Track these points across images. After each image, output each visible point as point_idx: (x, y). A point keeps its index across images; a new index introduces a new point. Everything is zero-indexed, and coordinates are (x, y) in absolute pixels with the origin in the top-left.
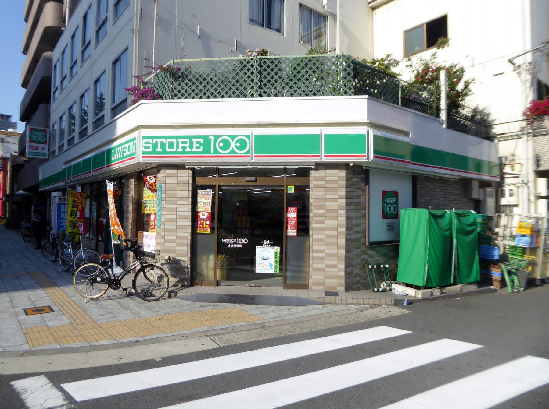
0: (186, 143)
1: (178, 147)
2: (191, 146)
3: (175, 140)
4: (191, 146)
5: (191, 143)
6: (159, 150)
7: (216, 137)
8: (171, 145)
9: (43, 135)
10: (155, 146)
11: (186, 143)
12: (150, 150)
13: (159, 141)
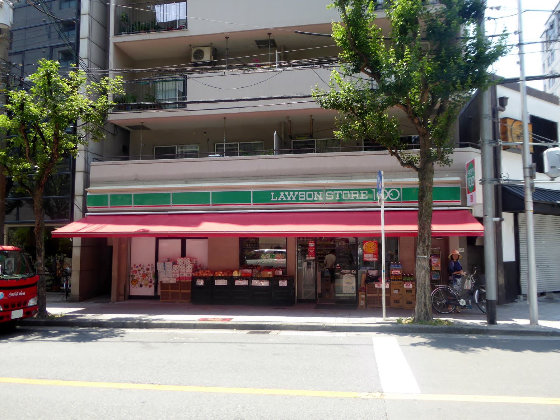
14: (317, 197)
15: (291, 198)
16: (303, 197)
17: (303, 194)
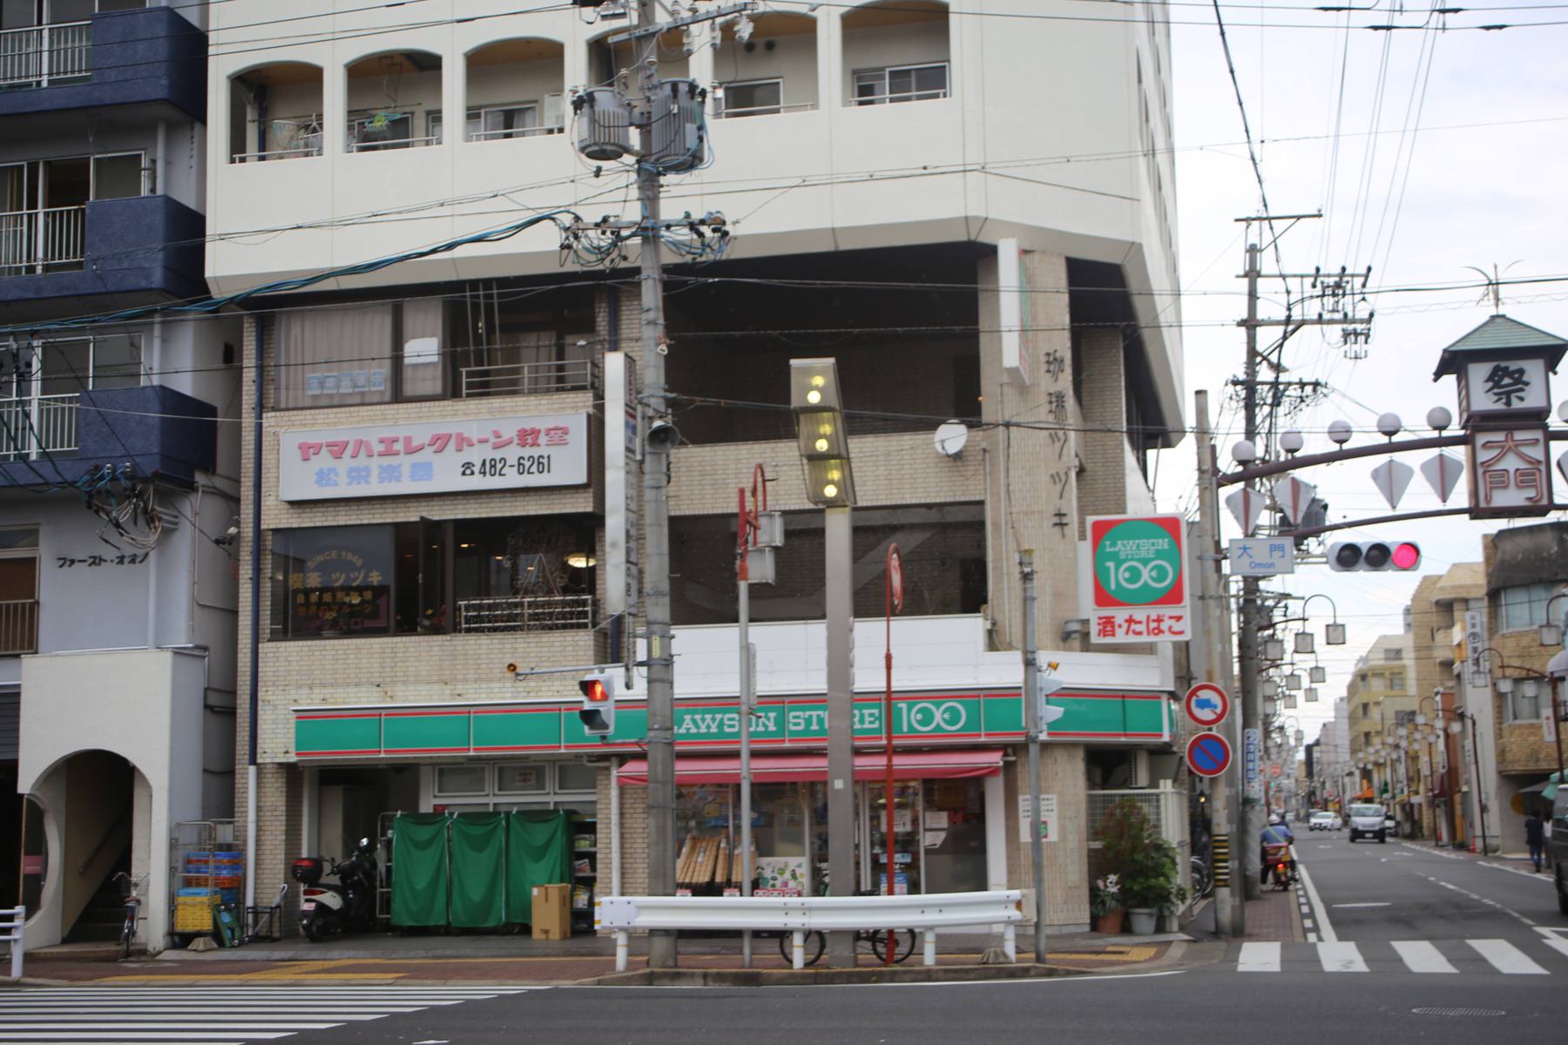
6: (815, 727)
9: (1159, 554)
12: (801, 728)
15: (708, 727)
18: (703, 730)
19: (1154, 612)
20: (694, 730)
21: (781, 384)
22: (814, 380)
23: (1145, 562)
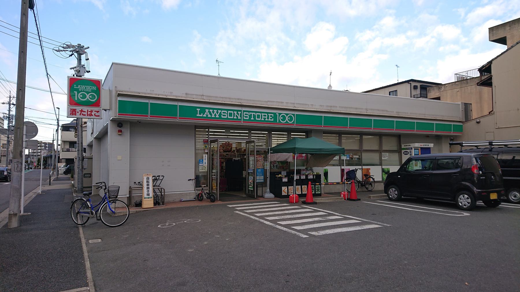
0: (266, 116)
1: (234, 116)
2: (268, 118)
3: (232, 112)
4: (268, 118)
5: (268, 116)
6: (252, 119)
7: (280, 114)
8: (258, 116)
9: (93, 91)
10: (250, 116)
11: (266, 116)
12: (248, 118)
13: (253, 114)
14: (237, 116)
15: (215, 115)
16: (225, 116)
17: (225, 113)
18: (213, 116)
19: (90, 109)
20: (209, 116)
21: (455, 198)
22: (464, 200)
23: (88, 93)
